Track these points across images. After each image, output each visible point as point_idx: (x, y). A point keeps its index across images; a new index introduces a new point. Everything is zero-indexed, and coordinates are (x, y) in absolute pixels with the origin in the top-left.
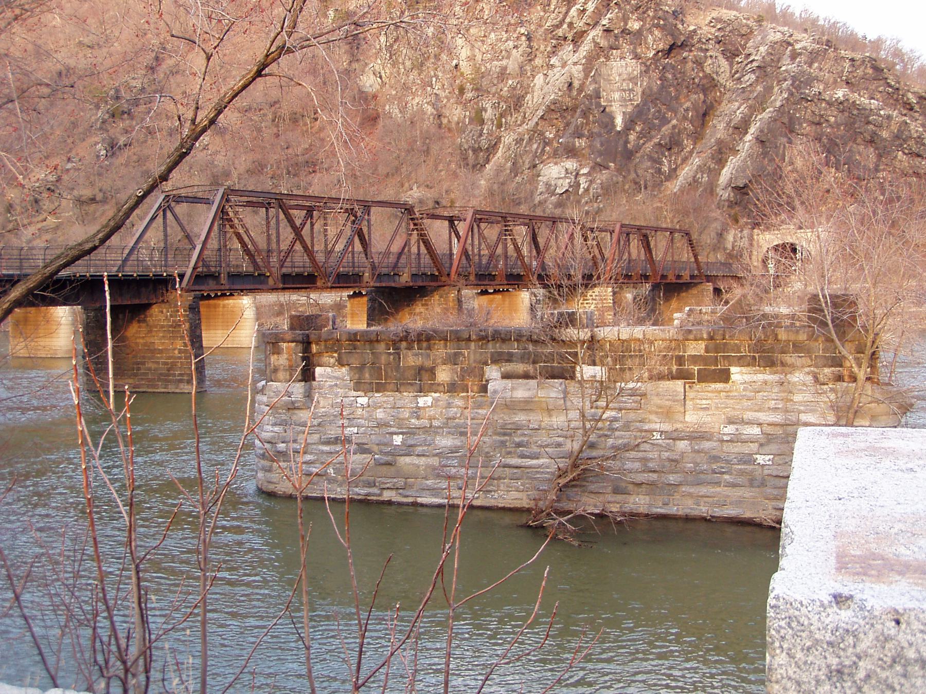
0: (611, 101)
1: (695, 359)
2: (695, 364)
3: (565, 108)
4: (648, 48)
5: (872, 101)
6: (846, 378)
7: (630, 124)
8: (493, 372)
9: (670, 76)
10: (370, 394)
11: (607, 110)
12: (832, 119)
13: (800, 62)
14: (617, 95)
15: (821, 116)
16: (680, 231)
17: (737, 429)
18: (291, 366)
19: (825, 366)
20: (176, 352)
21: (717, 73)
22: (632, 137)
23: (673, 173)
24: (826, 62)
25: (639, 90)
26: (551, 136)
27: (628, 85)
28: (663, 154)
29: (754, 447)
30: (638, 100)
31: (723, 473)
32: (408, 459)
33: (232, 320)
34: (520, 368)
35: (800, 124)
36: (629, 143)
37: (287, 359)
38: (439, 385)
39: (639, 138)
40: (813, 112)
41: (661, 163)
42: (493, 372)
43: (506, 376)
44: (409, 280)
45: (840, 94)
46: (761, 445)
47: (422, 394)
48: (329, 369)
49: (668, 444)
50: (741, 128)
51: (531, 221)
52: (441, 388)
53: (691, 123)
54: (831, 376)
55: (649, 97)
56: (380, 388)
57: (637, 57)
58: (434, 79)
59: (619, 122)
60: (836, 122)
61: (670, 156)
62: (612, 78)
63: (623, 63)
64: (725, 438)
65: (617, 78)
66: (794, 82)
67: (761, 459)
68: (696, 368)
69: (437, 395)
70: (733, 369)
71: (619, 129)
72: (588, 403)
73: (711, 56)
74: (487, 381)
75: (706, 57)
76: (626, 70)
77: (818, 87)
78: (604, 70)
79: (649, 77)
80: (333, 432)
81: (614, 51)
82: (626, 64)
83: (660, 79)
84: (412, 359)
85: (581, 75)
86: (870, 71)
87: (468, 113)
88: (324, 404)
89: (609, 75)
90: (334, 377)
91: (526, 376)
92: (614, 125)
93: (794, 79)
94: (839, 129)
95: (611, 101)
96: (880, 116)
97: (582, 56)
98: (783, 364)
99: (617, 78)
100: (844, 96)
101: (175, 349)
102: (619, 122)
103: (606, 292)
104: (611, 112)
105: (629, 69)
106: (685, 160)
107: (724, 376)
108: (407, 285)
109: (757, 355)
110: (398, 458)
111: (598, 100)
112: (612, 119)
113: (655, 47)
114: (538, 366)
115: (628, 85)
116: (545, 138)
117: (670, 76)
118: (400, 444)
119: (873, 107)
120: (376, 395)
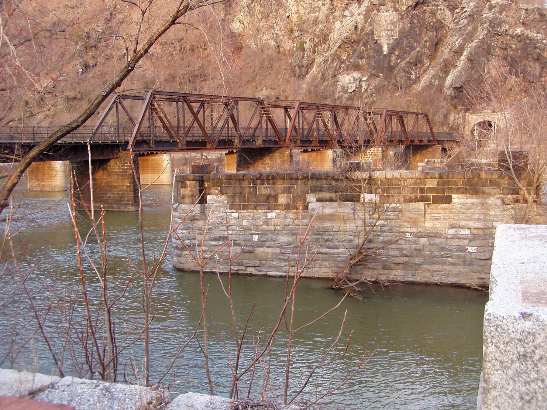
0: (380, 37)
1: (431, 190)
2: (431, 192)
3: (353, 41)
4: (403, 5)
5: (539, 35)
6: (521, 201)
7: (392, 51)
8: (311, 198)
9: (416, 21)
10: (239, 211)
11: (378, 42)
12: (514, 46)
13: (494, 12)
14: (384, 33)
15: (507, 44)
16: (421, 114)
17: (456, 231)
18: (192, 195)
19: (508, 194)
20: (125, 187)
21: (444, 19)
22: (393, 58)
23: (418, 80)
24: (510, 12)
25: (397, 30)
26: (345, 58)
27: (391, 27)
28: (412, 68)
29: (466, 242)
30: (397, 36)
31: (448, 257)
32: (261, 249)
33: (156, 169)
34: (328, 195)
35: (494, 49)
36: (391, 61)
37: (190, 191)
38: (280, 205)
39: (397, 59)
40: (502, 42)
41: (410, 73)
42: (311, 198)
43: (319, 200)
44: (261, 144)
45: (519, 31)
46: (470, 241)
47: (270, 211)
48: (215, 197)
49: (415, 240)
50: (459, 52)
51: (333, 109)
52: (281, 207)
53: (428, 49)
54: (511, 199)
55: (404, 34)
56: (245, 207)
57: (396, 10)
58: (275, 25)
59: (385, 49)
60: (516, 47)
61: (416, 69)
62: (381, 23)
63: (388, 14)
64: (449, 236)
65: (384, 23)
66: (490, 24)
67: (470, 249)
68: (432, 195)
69: (279, 211)
70: (454, 196)
71: (385, 53)
72: (367, 216)
73: (441, 9)
74: (308, 203)
75: (437, 10)
76: (389, 18)
77: (505, 27)
78: (376, 18)
79: (404, 22)
80: (217, 234)
81: (382, 7)
82: (390, 14)
83: (410, 23)
84: (263, 190)
85: (363, 21)
86: (537, 16)
87: (295, 45)
88: (212, 217)
89: (379, 21)
90: (218, 201)
91: (331, 200)
92: (382, 52)
93: (491, 22)
94: (517, 52)
95: (380, 37)
96: (543, 44)
97: (363, 10)
98: (483, 193)
99: (384, 23)
100: (521, 32)
101: (124, 186)
102: (385, 49)
103: (378, 150)
104: (381, 43)
105: (391, 17)
106: (425, 71)
107: (448, 200)
108: (260, 147)
109: (468, 187)
110: (256, 248)
111: (372, 36)
112: (381, 47)
113: (407, 4)
114: (338, 194)
115: (391, 27)
116: (341, 59)
117: (416, 21)
118: (257, 240)
119: (539, 38)
120: (243, 211)
